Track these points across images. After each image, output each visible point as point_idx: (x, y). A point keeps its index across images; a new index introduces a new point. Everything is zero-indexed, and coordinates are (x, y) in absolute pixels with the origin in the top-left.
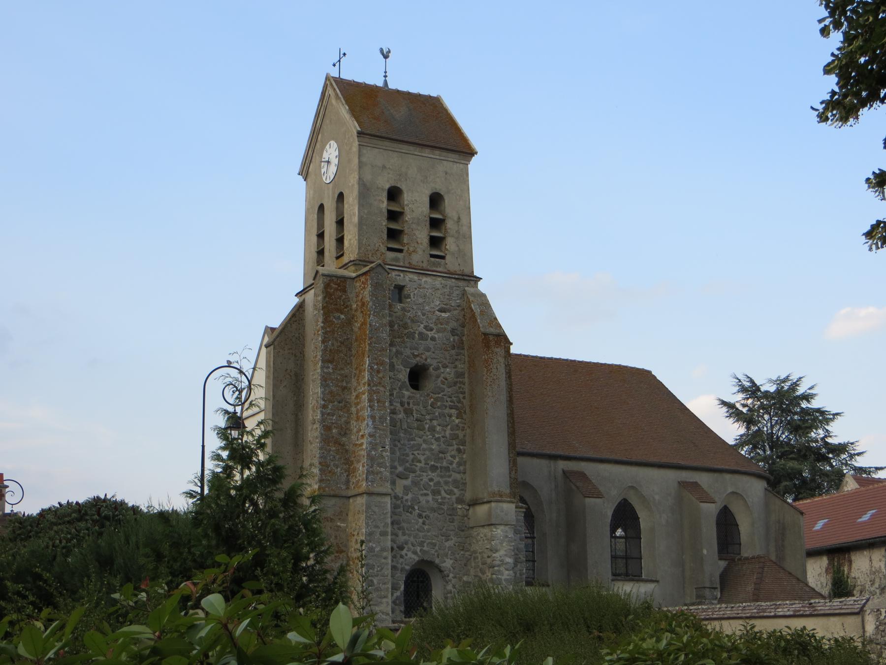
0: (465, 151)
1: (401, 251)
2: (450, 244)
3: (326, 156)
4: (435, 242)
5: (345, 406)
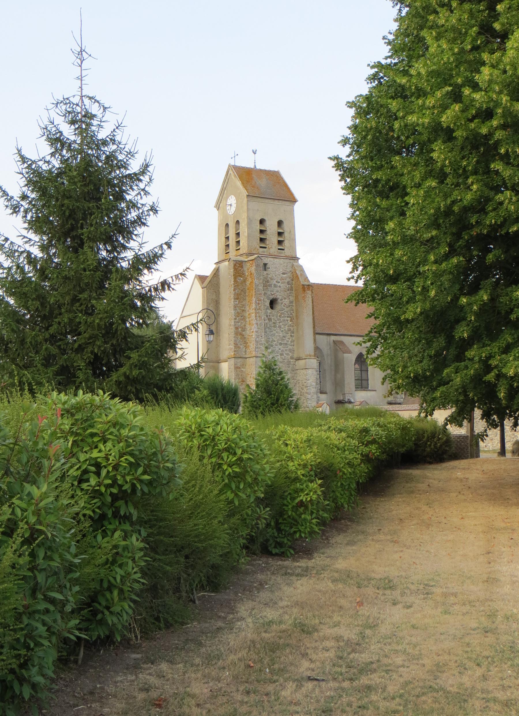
0: (291, 199)
1: (265, 248)
2: (286, 243)
3: (229, 202)
4: (280, 242)
5: (244, 318)
